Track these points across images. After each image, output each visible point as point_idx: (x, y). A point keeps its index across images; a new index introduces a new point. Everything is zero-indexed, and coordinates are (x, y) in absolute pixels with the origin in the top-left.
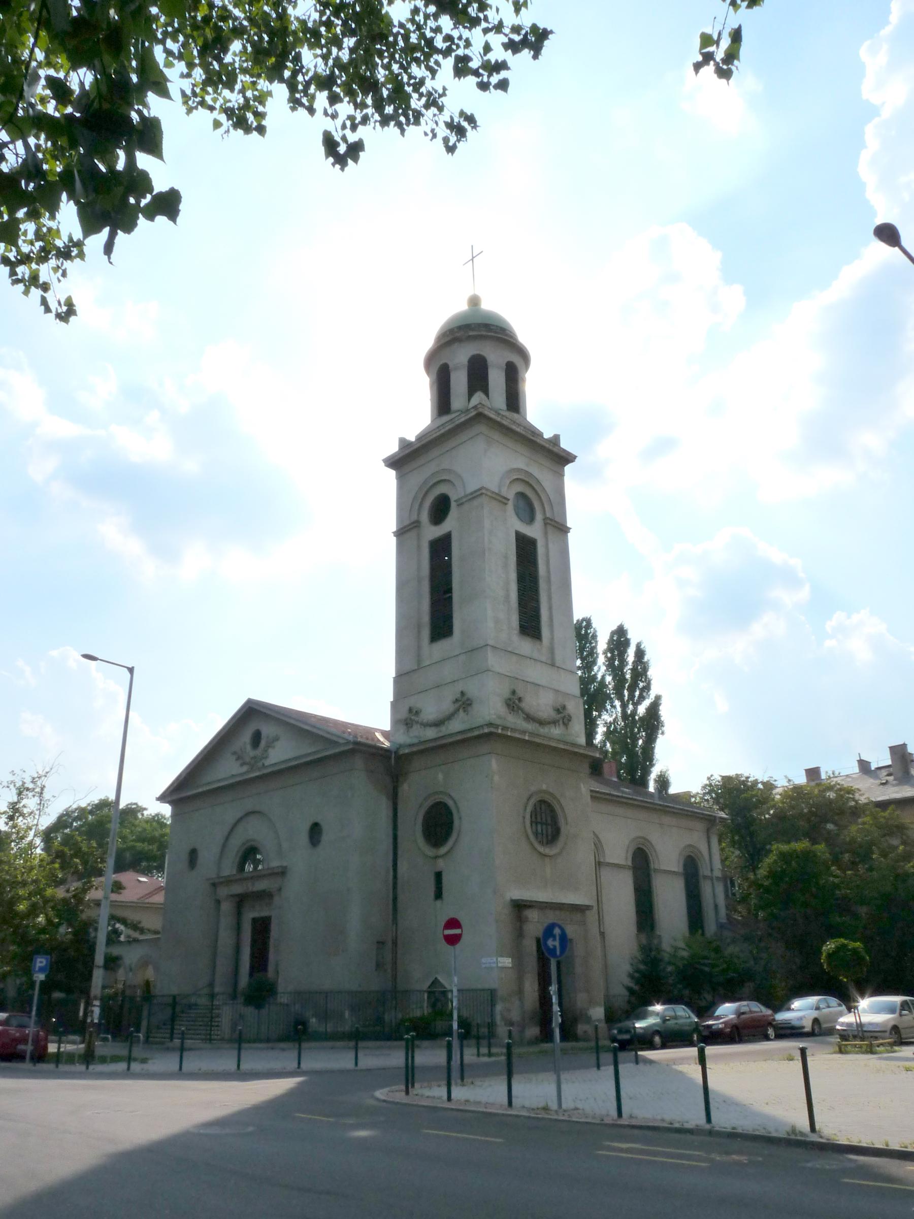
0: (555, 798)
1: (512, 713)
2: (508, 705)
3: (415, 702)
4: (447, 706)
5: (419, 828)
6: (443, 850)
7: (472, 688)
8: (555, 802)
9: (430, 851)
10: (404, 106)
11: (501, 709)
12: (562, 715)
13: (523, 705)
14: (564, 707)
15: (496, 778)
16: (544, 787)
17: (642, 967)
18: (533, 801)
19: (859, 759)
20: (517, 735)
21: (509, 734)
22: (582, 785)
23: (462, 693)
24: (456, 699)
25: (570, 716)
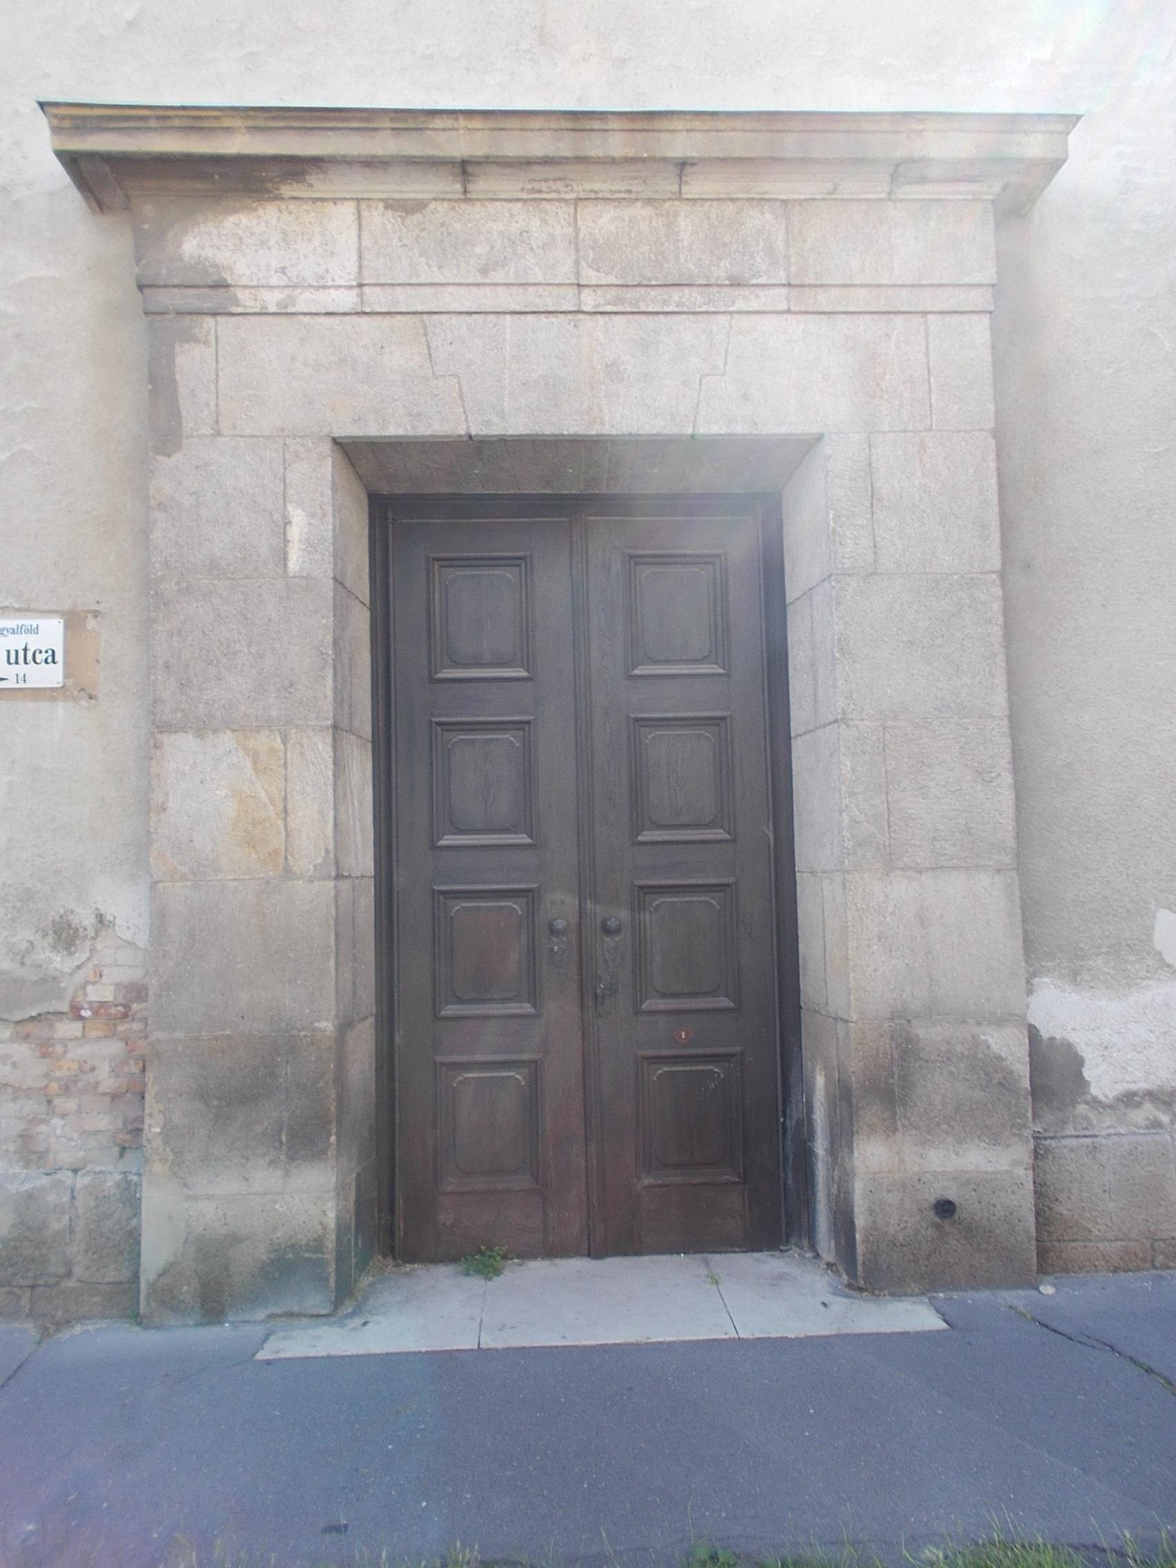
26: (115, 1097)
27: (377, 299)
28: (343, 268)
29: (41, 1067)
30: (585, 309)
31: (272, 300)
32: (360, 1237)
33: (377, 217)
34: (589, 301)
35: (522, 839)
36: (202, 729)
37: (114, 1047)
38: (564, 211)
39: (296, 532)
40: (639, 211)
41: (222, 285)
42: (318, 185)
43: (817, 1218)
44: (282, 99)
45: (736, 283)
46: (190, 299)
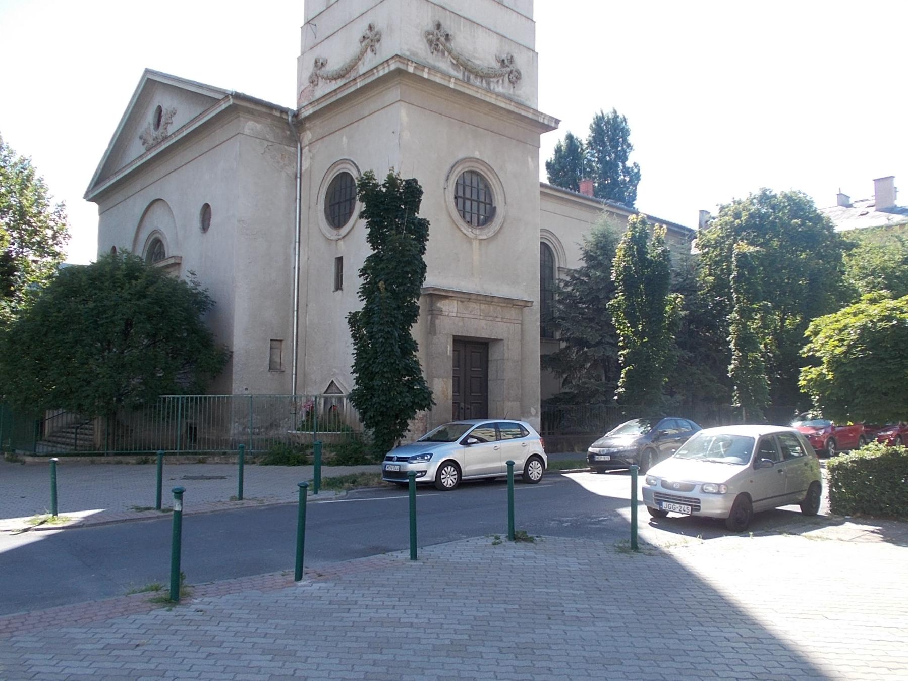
0: (491, 170)
1: (435, 52)
2: (430, 42)
3: (321, 52)
4: (355, 48)
5: (321, 206)
6: (344, 230)
7: (380, 19)
8: (491, 176)
9: (331, 233)
10: (640, 327)
11: (421, 50)
12: (509, 69)
13: (453, 45)
14: (511, 60)
15: (406, 135)
16: (477, 155)
17: (717, 418)
18: (459, 170)
19: (839, 193)
20: (438, 79)
21: (426, 76)
22: (530, 160)
23: (371, 28)
24: (364, 37)
25: (519, 73)
26: (422, 431)
27: (459, 315)
28: (455, 310)
29: (413, 427)
30: (245, 133)
31: (447, 313)
32: (345, 412)
33: (459, 303)
34: (481, 318)
35: (458, 394)
36: (438, 378)
37: (422, 424)
38: (478, 304)
39: (449, 349)
40: (487, 305)
41: (442, 311)
42: (453, 298)
43: (683, 565)
44: (894, 646)
45: (496, 317)
46: (437, 313)
